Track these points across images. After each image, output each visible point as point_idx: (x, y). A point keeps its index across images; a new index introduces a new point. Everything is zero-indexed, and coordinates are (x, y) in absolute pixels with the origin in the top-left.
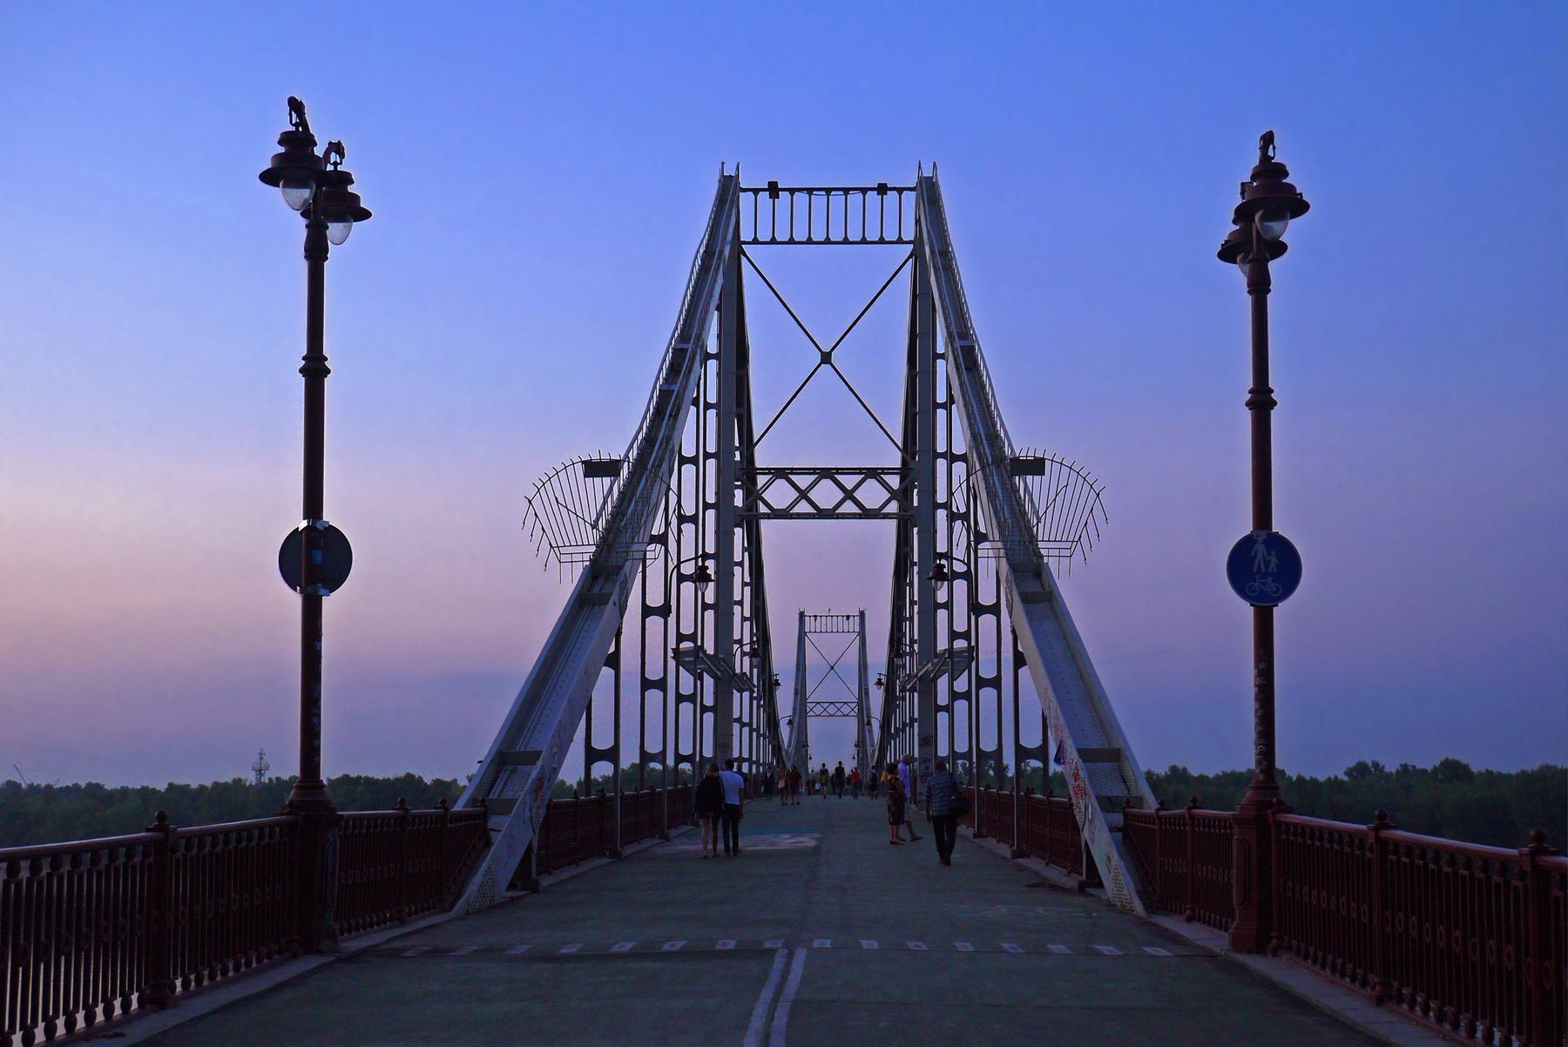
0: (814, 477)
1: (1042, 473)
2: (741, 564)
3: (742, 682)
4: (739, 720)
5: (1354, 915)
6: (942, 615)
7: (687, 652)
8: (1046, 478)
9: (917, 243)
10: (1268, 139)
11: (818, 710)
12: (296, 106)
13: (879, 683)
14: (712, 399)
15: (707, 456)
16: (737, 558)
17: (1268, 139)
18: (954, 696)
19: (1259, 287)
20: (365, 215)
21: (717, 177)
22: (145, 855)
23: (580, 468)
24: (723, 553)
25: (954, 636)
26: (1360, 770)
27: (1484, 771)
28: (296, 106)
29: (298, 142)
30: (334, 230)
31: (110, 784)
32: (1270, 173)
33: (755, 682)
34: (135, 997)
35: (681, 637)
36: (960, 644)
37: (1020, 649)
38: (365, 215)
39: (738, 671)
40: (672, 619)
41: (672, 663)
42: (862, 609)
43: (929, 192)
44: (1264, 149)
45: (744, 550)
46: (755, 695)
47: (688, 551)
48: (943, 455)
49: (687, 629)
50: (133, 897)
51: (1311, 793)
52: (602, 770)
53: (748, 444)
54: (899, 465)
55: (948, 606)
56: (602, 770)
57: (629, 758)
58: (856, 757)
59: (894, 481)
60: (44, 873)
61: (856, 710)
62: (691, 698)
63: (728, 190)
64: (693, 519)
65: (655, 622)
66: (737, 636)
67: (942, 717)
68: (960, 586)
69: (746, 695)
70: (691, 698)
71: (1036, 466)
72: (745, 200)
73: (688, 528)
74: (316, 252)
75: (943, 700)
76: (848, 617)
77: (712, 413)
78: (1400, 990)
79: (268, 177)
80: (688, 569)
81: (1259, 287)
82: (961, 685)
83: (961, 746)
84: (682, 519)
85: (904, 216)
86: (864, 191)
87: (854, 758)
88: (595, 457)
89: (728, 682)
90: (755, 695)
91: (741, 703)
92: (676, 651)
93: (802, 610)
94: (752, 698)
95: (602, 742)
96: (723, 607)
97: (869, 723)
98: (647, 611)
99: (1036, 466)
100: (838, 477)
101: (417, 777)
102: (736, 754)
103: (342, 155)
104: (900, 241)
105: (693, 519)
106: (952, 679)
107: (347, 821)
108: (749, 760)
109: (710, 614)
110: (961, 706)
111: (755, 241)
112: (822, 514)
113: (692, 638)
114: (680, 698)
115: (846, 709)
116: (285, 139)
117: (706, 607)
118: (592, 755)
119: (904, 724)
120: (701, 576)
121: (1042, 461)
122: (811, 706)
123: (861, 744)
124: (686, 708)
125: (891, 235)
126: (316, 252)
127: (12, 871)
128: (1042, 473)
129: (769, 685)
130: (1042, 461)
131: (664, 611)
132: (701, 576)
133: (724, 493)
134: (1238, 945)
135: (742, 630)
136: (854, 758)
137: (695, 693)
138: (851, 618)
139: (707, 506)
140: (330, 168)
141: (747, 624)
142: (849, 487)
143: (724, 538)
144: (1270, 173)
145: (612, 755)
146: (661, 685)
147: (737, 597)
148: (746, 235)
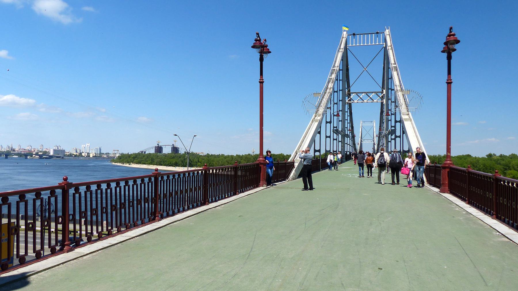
2: (347, 112)
3: (348, 136)
4: (347, 144)
5: (464, 184)
6: (390, 122)
7: (335, 130)
10: (451, 28)
12: (258, 34)
13: (377, 136)
14: (341, 78)
15: (340, 90)
16: (346, 111)
17: (451, 28)
18: (392, 139)
19: (449, 58)
20: (270, 52)
24: (343, 111)
25: (392, 127)
26: (490, 156)
28: (258, 34)
29: (258, 40)
30: (265, 56)
31: (226, 154)
33: (350, 136)
34: (232, 193)
35: (334, 127)
36: (393, 128)
38: (270, 52)
39: (346, 133)
40: (332, 124)
41: (332, 133)
45: (348, 109)
46: (350, 138)
47: (335, 110)
48: (390, 89)
49: (335, 126)
52: (317, 154)
53: (349, 86)
55: (391, 120)
56: (317, 154)
57: (323, 152)
60: (217, 172)
62: (336, 139)
64: (337, 104)
65: (328, 125)
66: (346, 127)
67: (389, 143)
68: (393, 116)
69: (348, 138)
70: (336, 139)
73: (336, 105)
74: (261, 60)
75: (390, 140)
77: (341, 82)
78: (471, 201)
80: (336, 114)
81: (449, 58)
82: (393, 137)
83: (398, 149)
89: (344, 136)
90: (350, 138)
91: (348, 140)
92: (333, 130)
94: (350, 139)
95: (317, 148)
96: (343, 121)
98: (327, 122)
102: (346, 150)
103: (266, 42)
105: (337, 104)
106: (392, 135)
108: (349, 152)
109: (340, 122)
110: (393, 141)
113: (336, 127)
114: (334, 139)
117: (339, 121)
118: (315, 151)
120: (338, 115)
126: (261, 60)
129: (353, 137)
131: (330, 122)
132: (338, 115)
133: (344, 98)
134: (440, 192)
135: (347, 125)
139: (340, 101)
140: (264, 44)
141: (349, 124)
143: (343, 106)
145: (319, 151)
146: (330, 137)
147: (346, 119)
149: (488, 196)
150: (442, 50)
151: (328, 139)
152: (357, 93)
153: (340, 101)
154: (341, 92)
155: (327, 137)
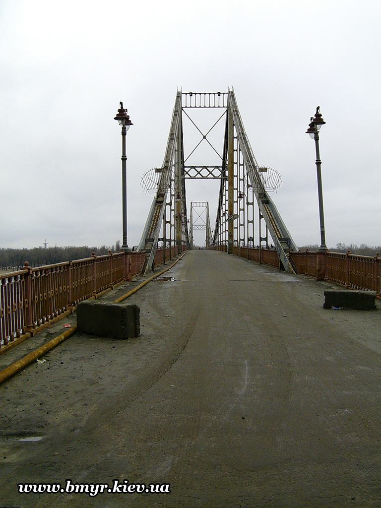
0: (202, 168)
1: (266, 171)
2: (226, 200)
8: (267, 173)
9: (228, 107)
10: (318, 108)
12: (121, 103)
15: (237, 150)
17: (318, 108)
19: (317, 139)
20: (325, 123)
21: (176, 92)
22: (21, 278)
23: (154, 170)
27: (309, 127)
28: (121, 103)
32: (318, 115)
37: (261, 214)
38: (325, 123)
41: (246, 193)
43: (231, 95)
44: (317, 110)
52: (264, 243)
54: (222, 165)
59: (221, 168)
60: (6, 284)
63: (179, 96)
71: (265, 170)
72: (183, 96)
74: (124, 134)
77: (235, 161)
79: (115, 119)
84: (248, 203)
85: (224, 100)
86: (214, 94)
88: (158, 168)
99: (265, 170)
100: (208, 168)
104: (224, 107)
105: (240, 225)
107: (64, 266)
111: (186, 107)
112: (203, 178)
116: (119, 110)
119: (223, 232)
121: (266, 169)
123: (208, 237)
126: (124, 134)
127: (3, 282)
128: (266, 171)
130: (266, 169)
142: (211, 171)
144: (318, 115)
147: (227, 202)
149: (45, 294)
150: (116, 116)
151: (250, 219)
152: (215, 178)
153: (237, 228)
154: (235, 148)
155: (252, 222)
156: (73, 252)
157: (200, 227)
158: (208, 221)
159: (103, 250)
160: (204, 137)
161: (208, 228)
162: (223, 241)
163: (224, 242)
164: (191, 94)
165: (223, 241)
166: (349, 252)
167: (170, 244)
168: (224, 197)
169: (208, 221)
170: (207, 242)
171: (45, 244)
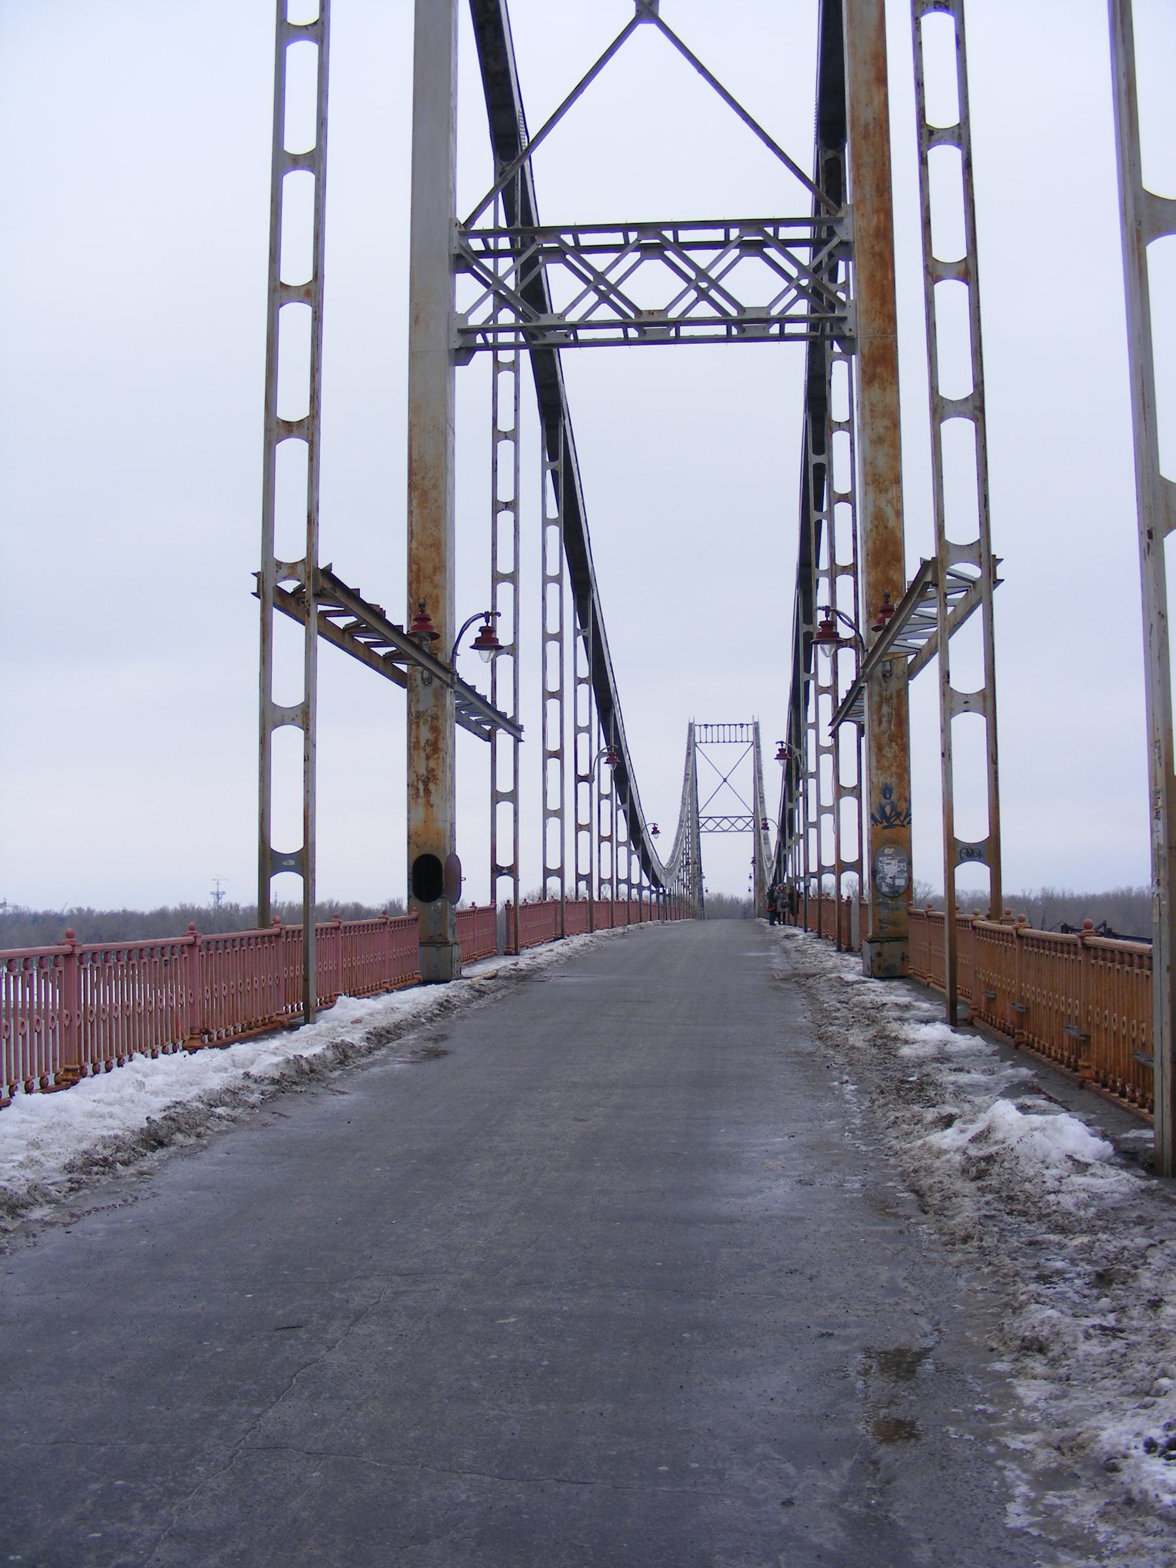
11: (711, 825)
40: (595, 784)
42: (756, 720)
50: (140, 1022)
51: (1022, 903)
58: (753, 876)
61: (752, 824)
62: (609, 839)
63: (691, 727)
65: (584, 786)
70: (609, 839)
72: (697, 728)
76: (742, 725)
86: (736, 725)
87: (750, 877)
93: (691, 722)
97: (766, 827)
100: (790, 250)
101: (86, 909)
115: (740, 824)
122: (702, 821)
124: (606, 846)
125: (745, 740)
136: (750, 877)
137: (611, 836)
138: (745, 726)
148: (697, 740)
156: (967, 895)
157: (725, 824)
158: (759, 797)
159: (143, 914)
160: (725, 780)
161: (760, 826)
162: (822, 869)
163: (829, 880)
164: (706, 726)
165: (822, 869)
166: (930, 907)
167: (640, 894)
168: (811, 733)
169: (759, 797)
170: (759, 882)
171: (218, 896)
